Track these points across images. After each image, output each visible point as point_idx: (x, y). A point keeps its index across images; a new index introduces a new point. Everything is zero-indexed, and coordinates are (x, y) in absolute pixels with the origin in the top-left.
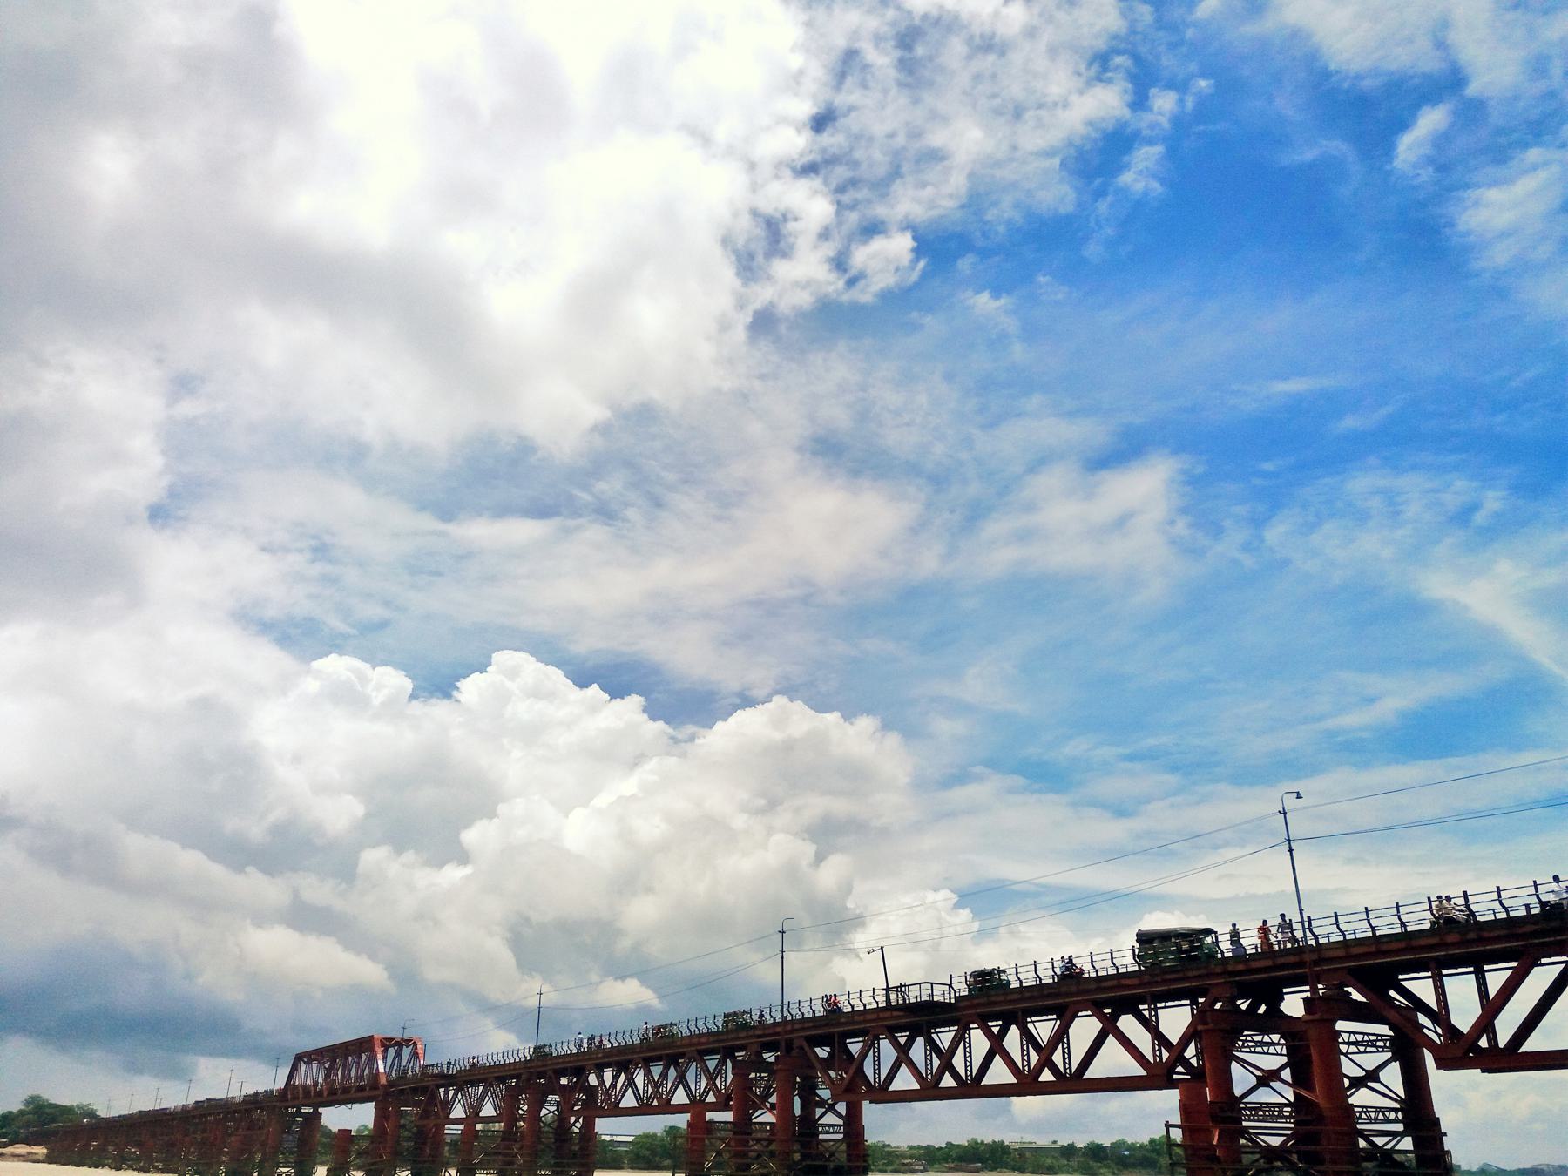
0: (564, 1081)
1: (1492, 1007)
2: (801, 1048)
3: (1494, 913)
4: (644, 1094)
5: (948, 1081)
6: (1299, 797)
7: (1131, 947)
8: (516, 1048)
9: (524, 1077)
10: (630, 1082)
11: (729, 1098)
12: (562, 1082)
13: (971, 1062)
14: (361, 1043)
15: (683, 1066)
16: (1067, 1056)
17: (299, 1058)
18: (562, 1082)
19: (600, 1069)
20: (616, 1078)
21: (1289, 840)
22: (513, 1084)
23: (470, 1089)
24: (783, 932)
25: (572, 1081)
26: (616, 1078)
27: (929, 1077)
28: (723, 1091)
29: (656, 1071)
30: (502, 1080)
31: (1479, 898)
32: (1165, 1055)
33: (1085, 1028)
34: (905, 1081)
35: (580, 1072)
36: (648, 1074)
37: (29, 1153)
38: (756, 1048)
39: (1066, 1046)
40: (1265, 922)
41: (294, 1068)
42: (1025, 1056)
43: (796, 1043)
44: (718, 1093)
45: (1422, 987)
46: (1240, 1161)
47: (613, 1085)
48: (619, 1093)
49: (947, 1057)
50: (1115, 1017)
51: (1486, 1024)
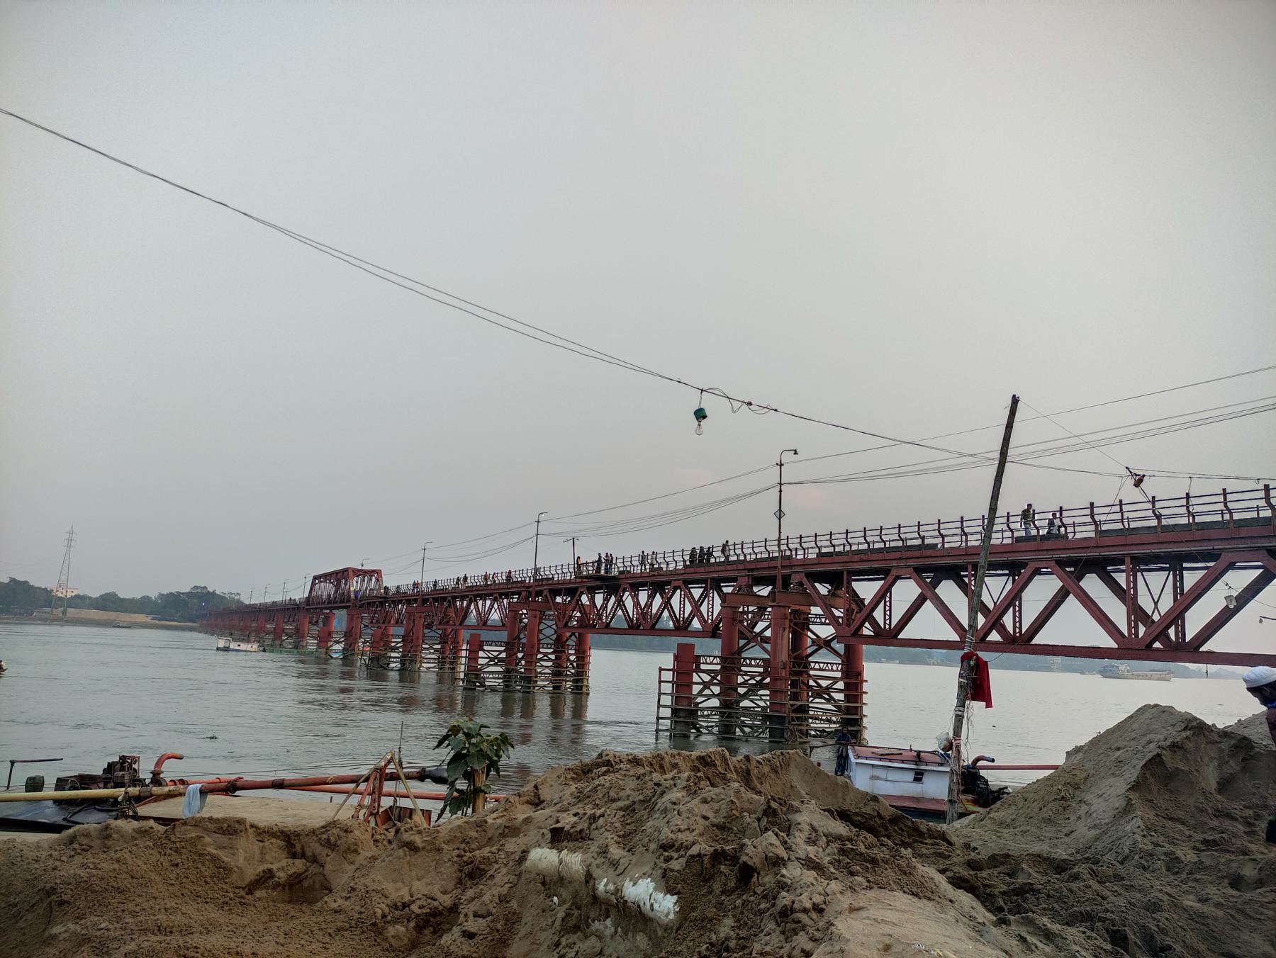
0: (559, 599)
1: (1185, 601)
2: (801, 584)
3: (1258, 511)
4: (708, 616)
5: (696, 624)
6: (796, 453)
7: (863, 530)
8: (452, 578)
9: (524, 594)
10: (620, 604)
11: (716, 628)
12: (557, 600)
13: (890, 616)
14: (337, 573)
15: (669, 592)
16: (888, 613)
17: (315, 578)
18: (557, 600)
19: (592, 591)
20: (606, 600)
21: (781, 484)
22: (515, 600)
23: (505, 600)
24: (538, 522)
25: (565, 600)
26: (606, 600)
27: (710, 621)
28: (710, 621)
29: (643, 597)
30: (507, 595)
31: (838, 536)
32: (981, 620)
33: (1041, 590)
34: (994, 636)
35: (838, 579)
36: (635, 598)
37: (386, 694)
38: (743, 581)
39: (1017, 609)
40: (727, 542)
41: (313, 585)
42: (973, 619)
43: (795, 579)
44: (703, 621)
45: (866, 589)
46: (845, 695)
47: (604, 607)
48: (611, 612)
49: (697, 605)
50: (935, 584)
51: (1177, 617)
